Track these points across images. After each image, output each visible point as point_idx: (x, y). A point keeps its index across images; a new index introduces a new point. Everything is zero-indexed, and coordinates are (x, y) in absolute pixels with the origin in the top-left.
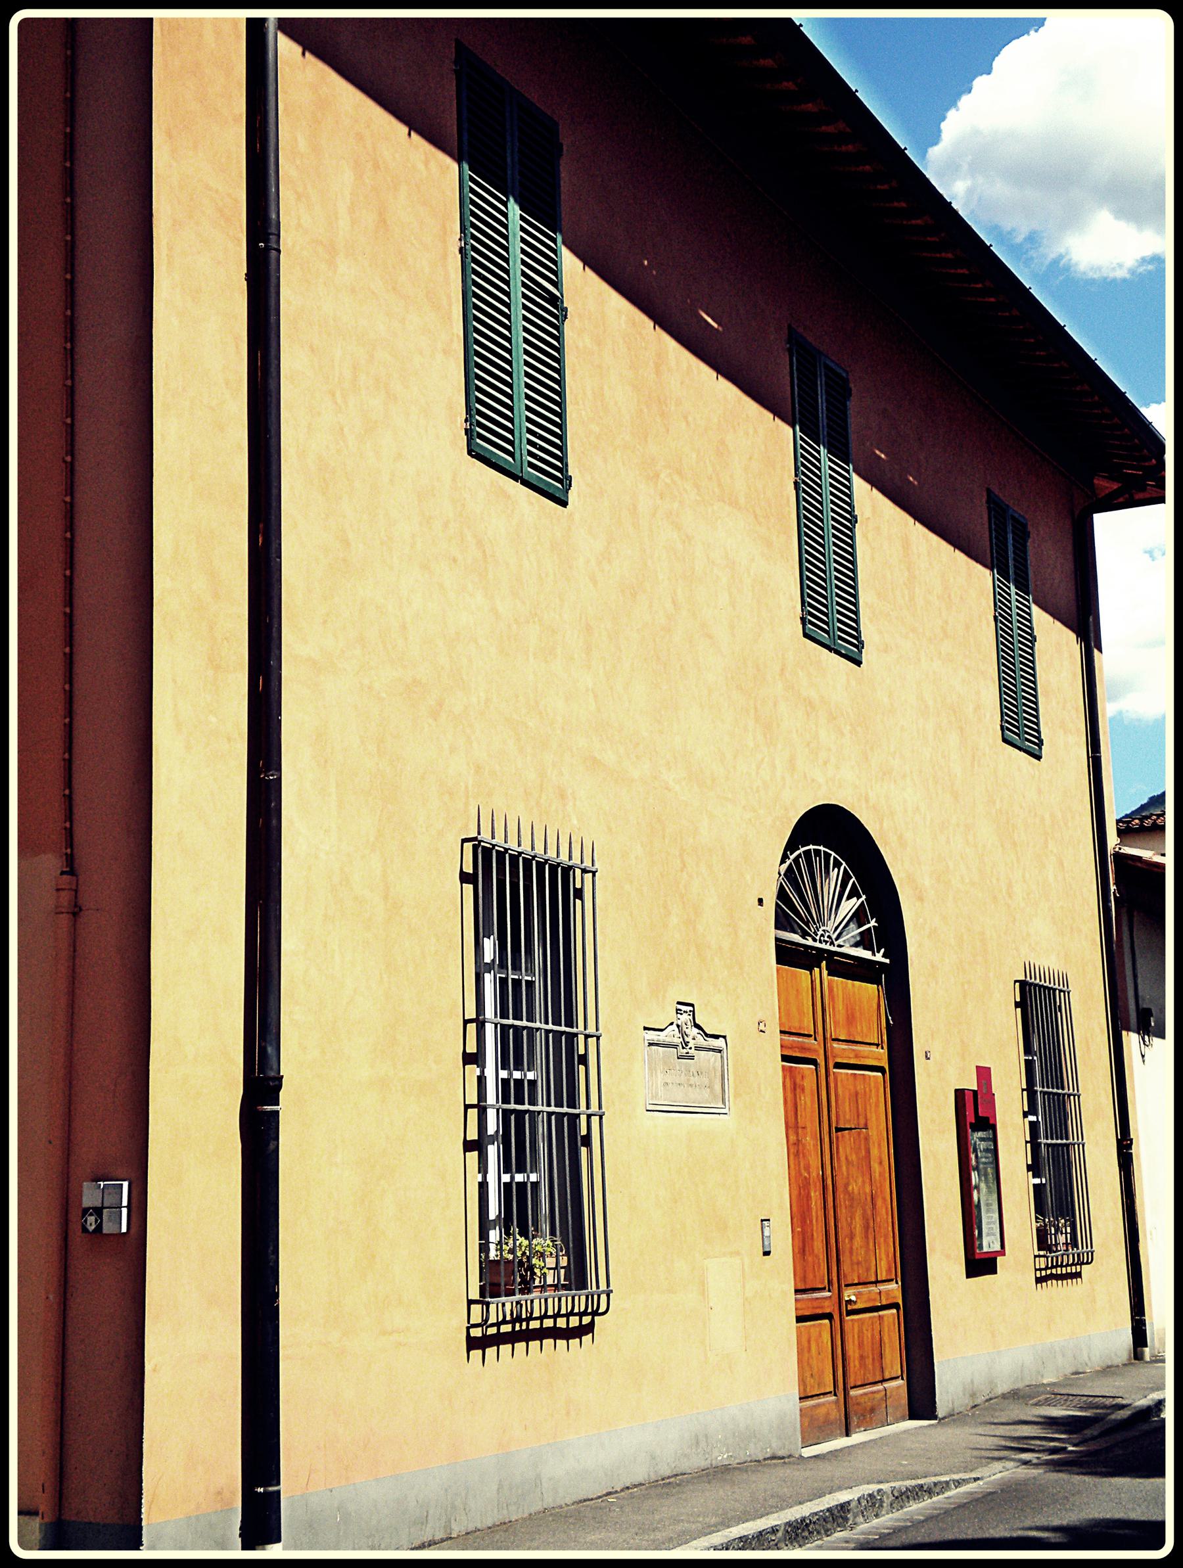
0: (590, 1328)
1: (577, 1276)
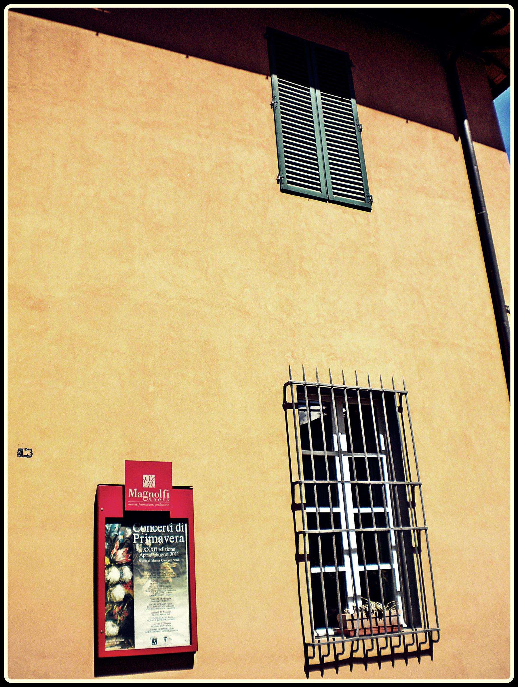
0: (429, 652)
1: (414, 619)
